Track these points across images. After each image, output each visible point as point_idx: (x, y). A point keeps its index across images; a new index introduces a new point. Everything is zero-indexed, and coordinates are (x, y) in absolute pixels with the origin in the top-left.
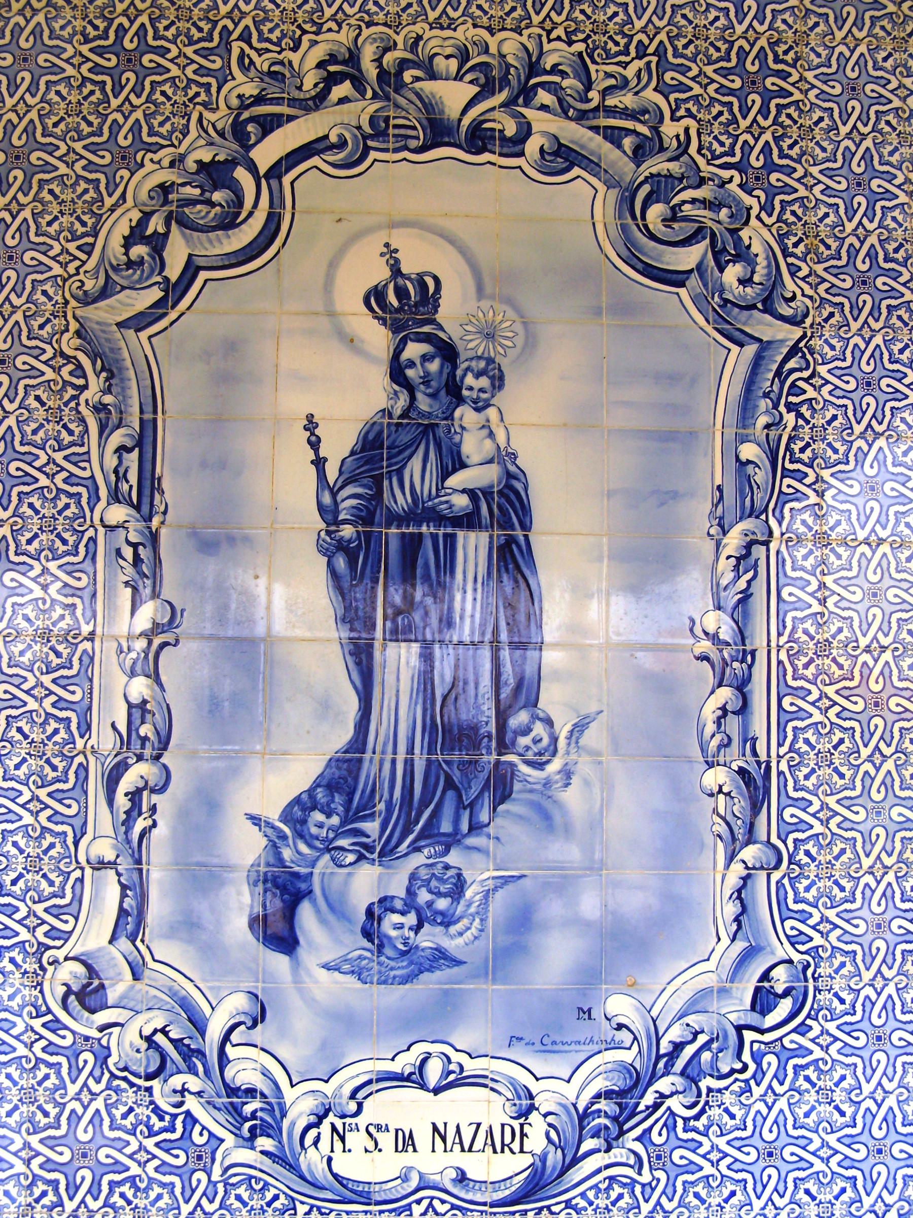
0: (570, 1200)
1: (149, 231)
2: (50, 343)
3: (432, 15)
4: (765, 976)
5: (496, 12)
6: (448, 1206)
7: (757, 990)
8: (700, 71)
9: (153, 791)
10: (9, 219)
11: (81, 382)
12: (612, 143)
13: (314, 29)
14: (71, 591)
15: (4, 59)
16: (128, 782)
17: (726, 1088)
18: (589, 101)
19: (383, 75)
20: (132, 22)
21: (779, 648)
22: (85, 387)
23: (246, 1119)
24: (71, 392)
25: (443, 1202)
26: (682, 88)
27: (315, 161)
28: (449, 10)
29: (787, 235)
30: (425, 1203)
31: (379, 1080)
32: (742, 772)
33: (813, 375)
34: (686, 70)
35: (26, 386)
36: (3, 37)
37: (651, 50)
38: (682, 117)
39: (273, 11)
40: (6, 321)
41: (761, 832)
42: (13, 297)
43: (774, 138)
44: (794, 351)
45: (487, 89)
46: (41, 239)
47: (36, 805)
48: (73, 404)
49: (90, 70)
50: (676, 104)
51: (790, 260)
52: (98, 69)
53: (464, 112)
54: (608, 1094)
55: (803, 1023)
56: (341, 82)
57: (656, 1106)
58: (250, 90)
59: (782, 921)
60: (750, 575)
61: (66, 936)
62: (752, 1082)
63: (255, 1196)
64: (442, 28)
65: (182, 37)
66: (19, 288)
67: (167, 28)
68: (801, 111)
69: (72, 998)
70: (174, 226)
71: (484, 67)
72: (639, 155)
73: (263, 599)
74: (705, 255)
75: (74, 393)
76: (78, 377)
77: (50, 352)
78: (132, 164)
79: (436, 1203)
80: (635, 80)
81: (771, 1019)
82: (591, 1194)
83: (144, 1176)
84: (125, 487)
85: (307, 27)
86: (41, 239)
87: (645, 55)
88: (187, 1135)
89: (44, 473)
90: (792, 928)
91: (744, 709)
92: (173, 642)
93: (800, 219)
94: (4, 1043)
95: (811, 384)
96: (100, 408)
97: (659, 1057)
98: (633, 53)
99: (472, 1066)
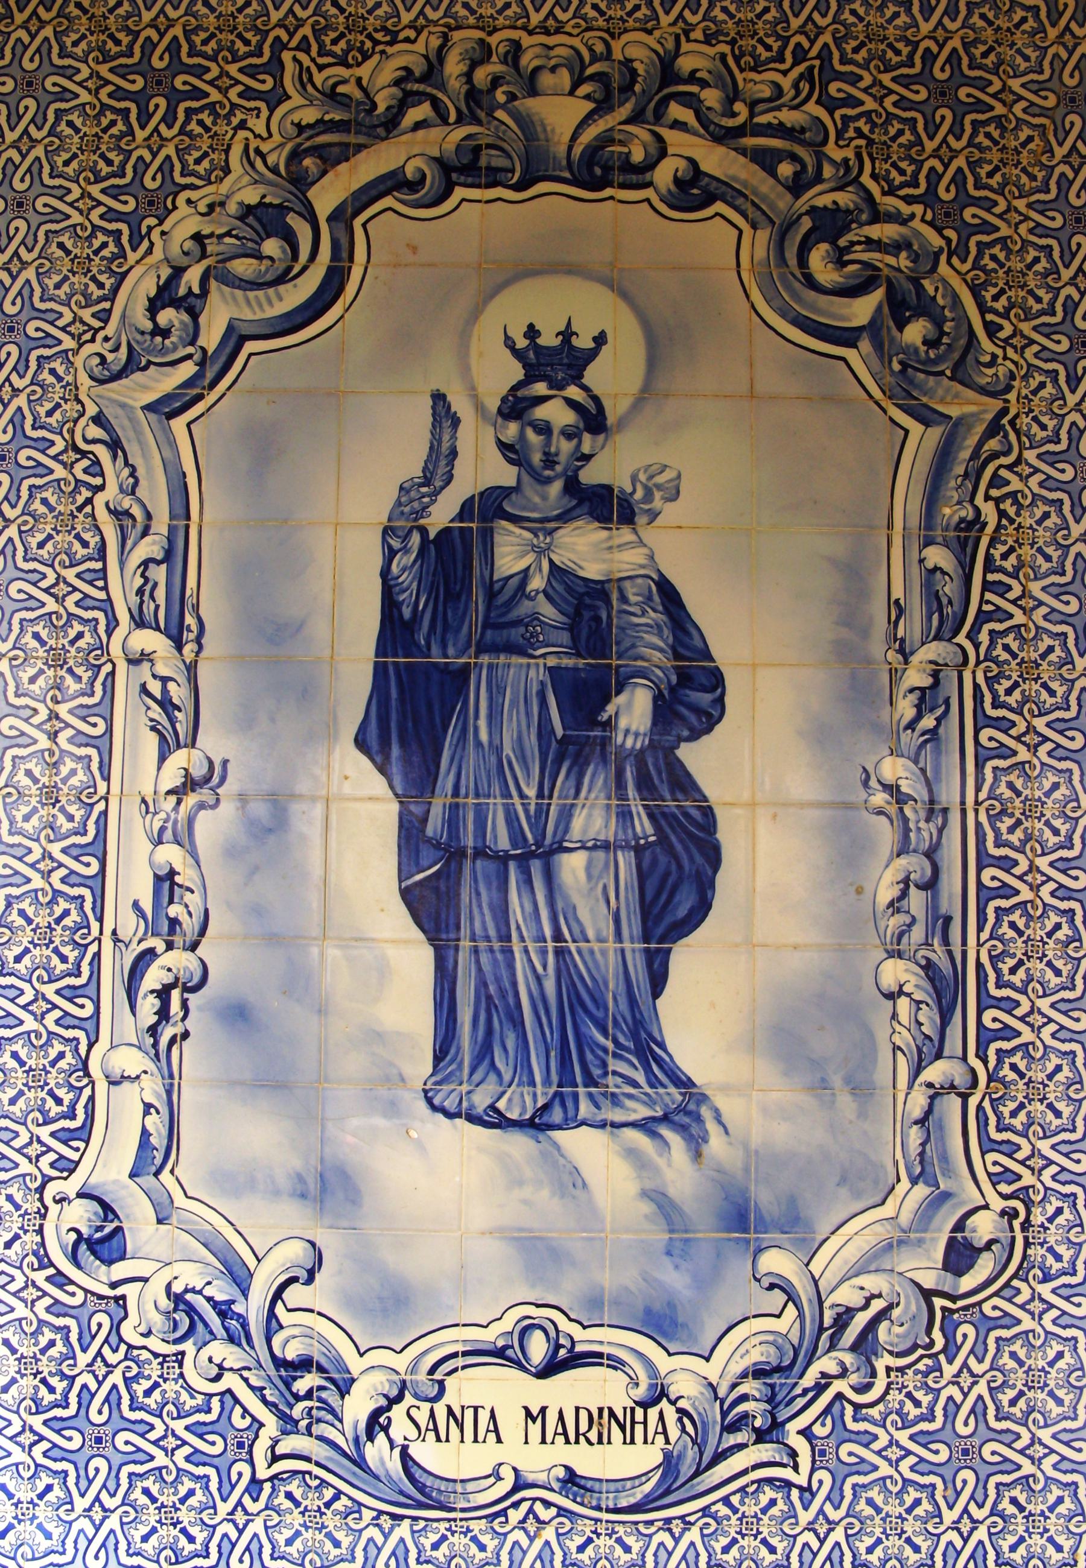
0: (708, 1507)
1: (182, 292)
2: (61, 434)
3: (536, 18)
4: (959, 1226)
5: (617, 12)
6: (553, 1511)
7: (951, 1243)
8: (875, 79)
9: (186, 989)
10: (7, 281)
11: (98, 481)
12: (764, 169)
13: (388, 38)
14: (84, 740)
15: (4, 84)
16: (154, 977)
17: (909, 1366)
18: (734, 115)
19: (473, 95)
20: (162, 35)
21: (977, 803)
22: (101, 488)
23: (298, 1398)
24: (86, 494)
25: (547, 1504)
26: (851, 101)
27: (387, 202)
28: (557, 11)
29: (985, 285)
30: (525, 1506)
31: (465, 1354)
32: (929, 967)
33: (1019, 461)
34: (857, 79)
35: (14, 758)
36: (3, 58)
37: (814, 53)
38: (852, 139)
39: (337, 17)
40: (6, 406)
41: (953, 1044)
42: (14, 378)
43: (969, 163)
44: (994, 429)
45: (602, 106)
46: (57, 182)
47: (39, 1012)
48: (88, 509)
49: (102, 217)
50: (843, 123)
51: (989, 317)
52: (120, 94)
53: (574, 138)
54: (758, 1372)
55: (1007, 1285)
56: (420, 103)
57: (819, 1389)
58: (309, 116)
59: (983, 1154)
60: (939, 712)
61: (72, 1166)
62: (942, 1357)
63: (310, 1495)
64: (547, 33)
65: (223, 112)
66: (39, 120)
67: (198, 161)
68: (1030, 918)
69: (83, 1247)
70: (213, 284)
71: (600, 78)
72: (797, 187)
73: (317, 872)
74: (879, 309)
75: (89, 494)
76: (94, 476)
77: (60, 445)
78: (161, 211)
79: (538, 1507)
80: (793, 92)
81: (967, 1282)
82: (735, 1500)
83: (172, 1466)
84: (149, 608)
85: (379, 36)
86: (57, 182)
87: (805, 60)
88: (225, 1413)
89: (69, 333)
90: (995, 1163)
91: (931, 885)
92: (212, 802)
93: (1002, 266)
94: (4, 1157)
95: (1016, 473)
96: (119, 514)
97: (821, 1329)
98: (789, 60)
99: (586, 1339)
